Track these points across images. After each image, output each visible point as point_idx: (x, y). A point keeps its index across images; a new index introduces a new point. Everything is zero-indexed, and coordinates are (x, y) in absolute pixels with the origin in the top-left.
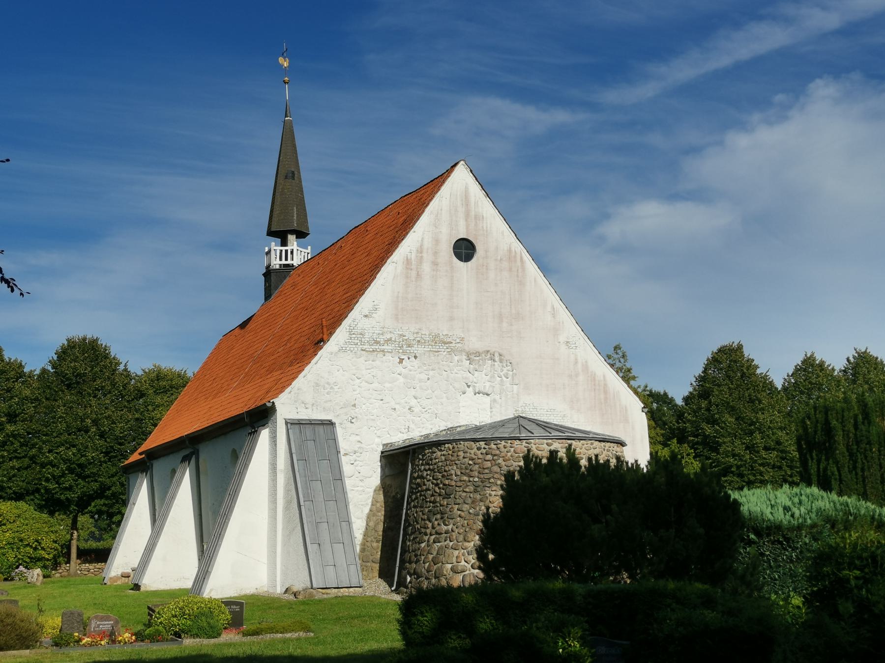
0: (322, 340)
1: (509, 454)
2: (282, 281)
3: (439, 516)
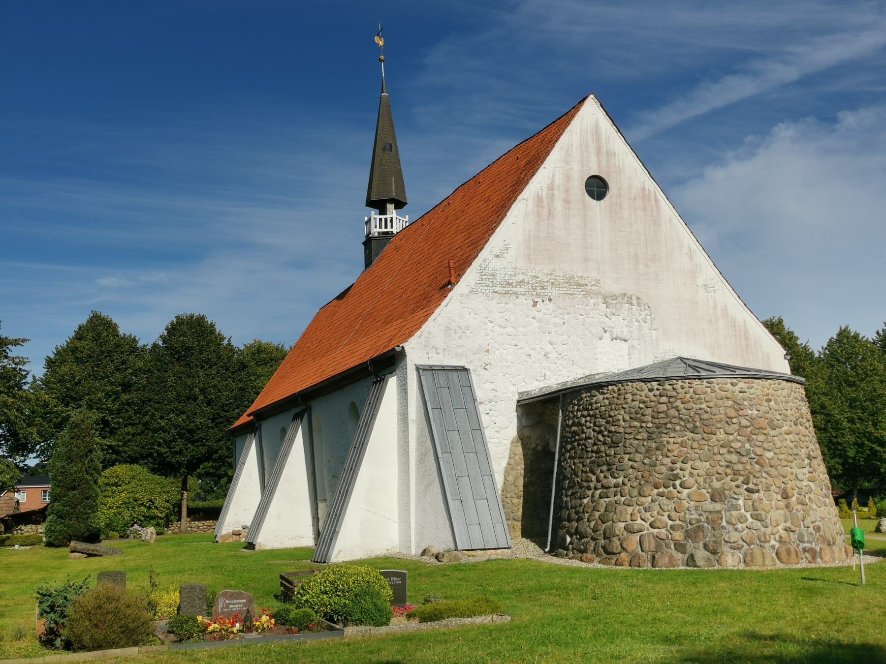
0: (450, 283)
1: (688, 396)
2: (382, 248)
3: (605, 468)
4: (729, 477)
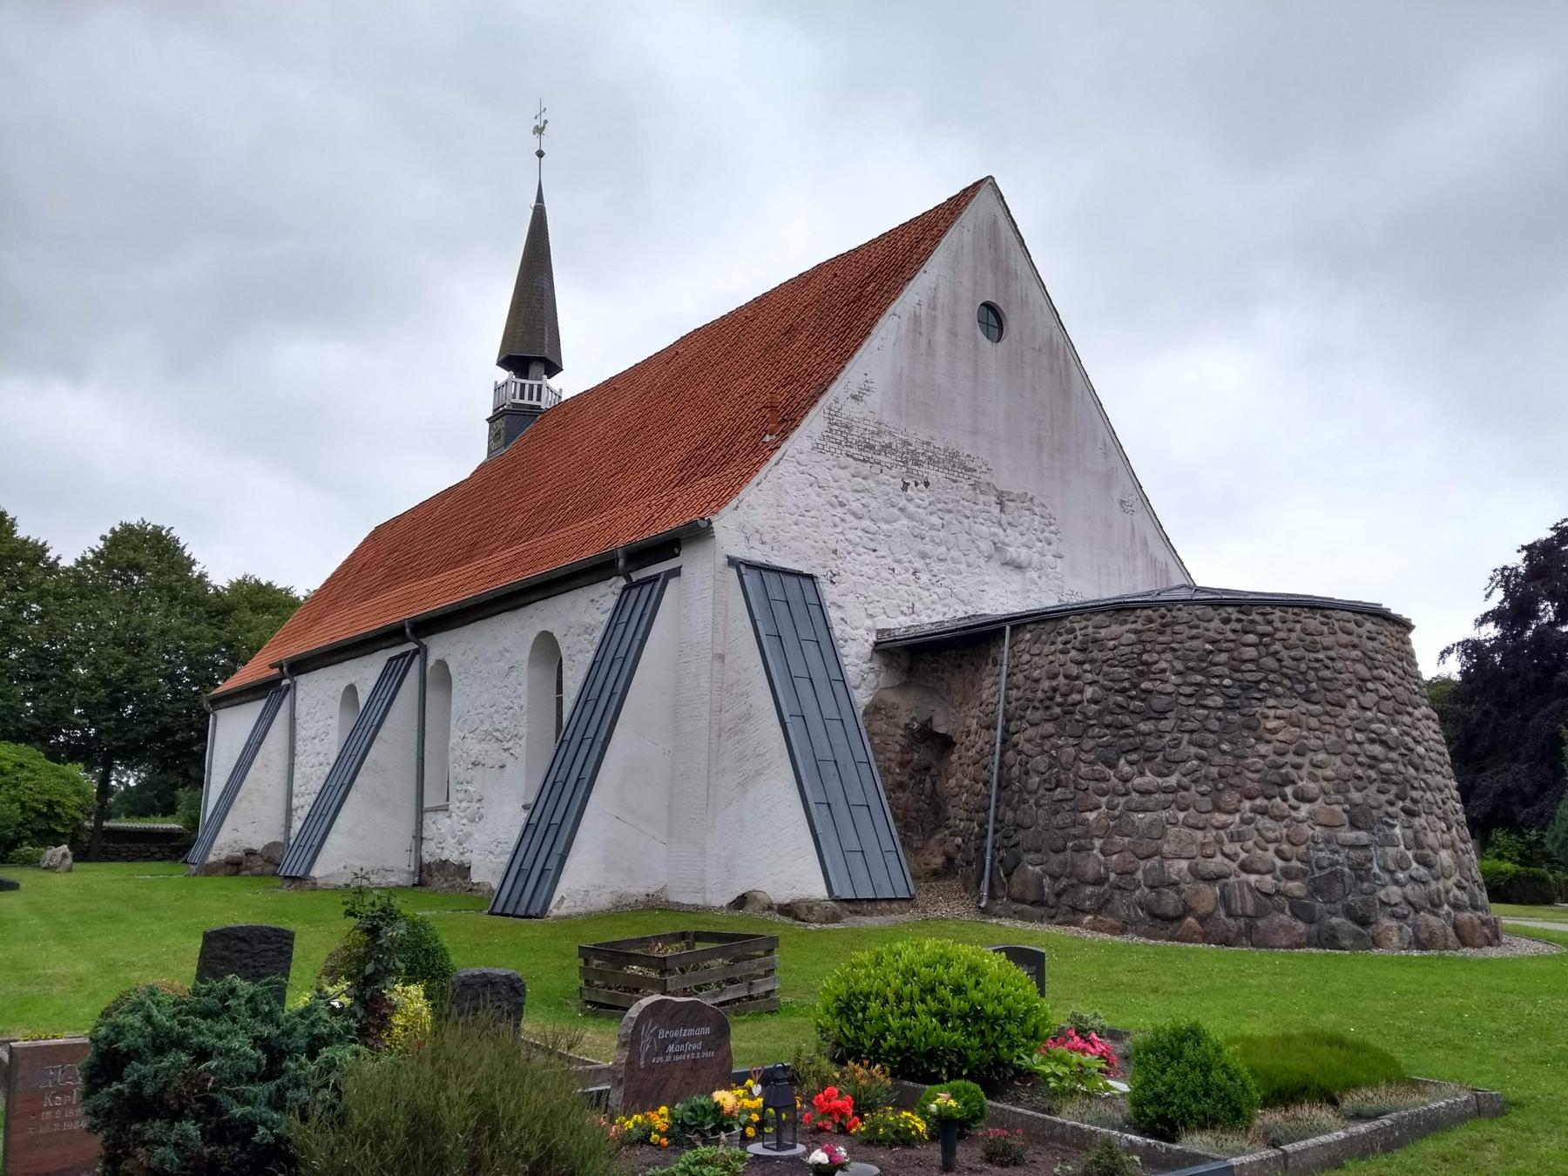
1: (1293, 635)
4: (1374, 787)
